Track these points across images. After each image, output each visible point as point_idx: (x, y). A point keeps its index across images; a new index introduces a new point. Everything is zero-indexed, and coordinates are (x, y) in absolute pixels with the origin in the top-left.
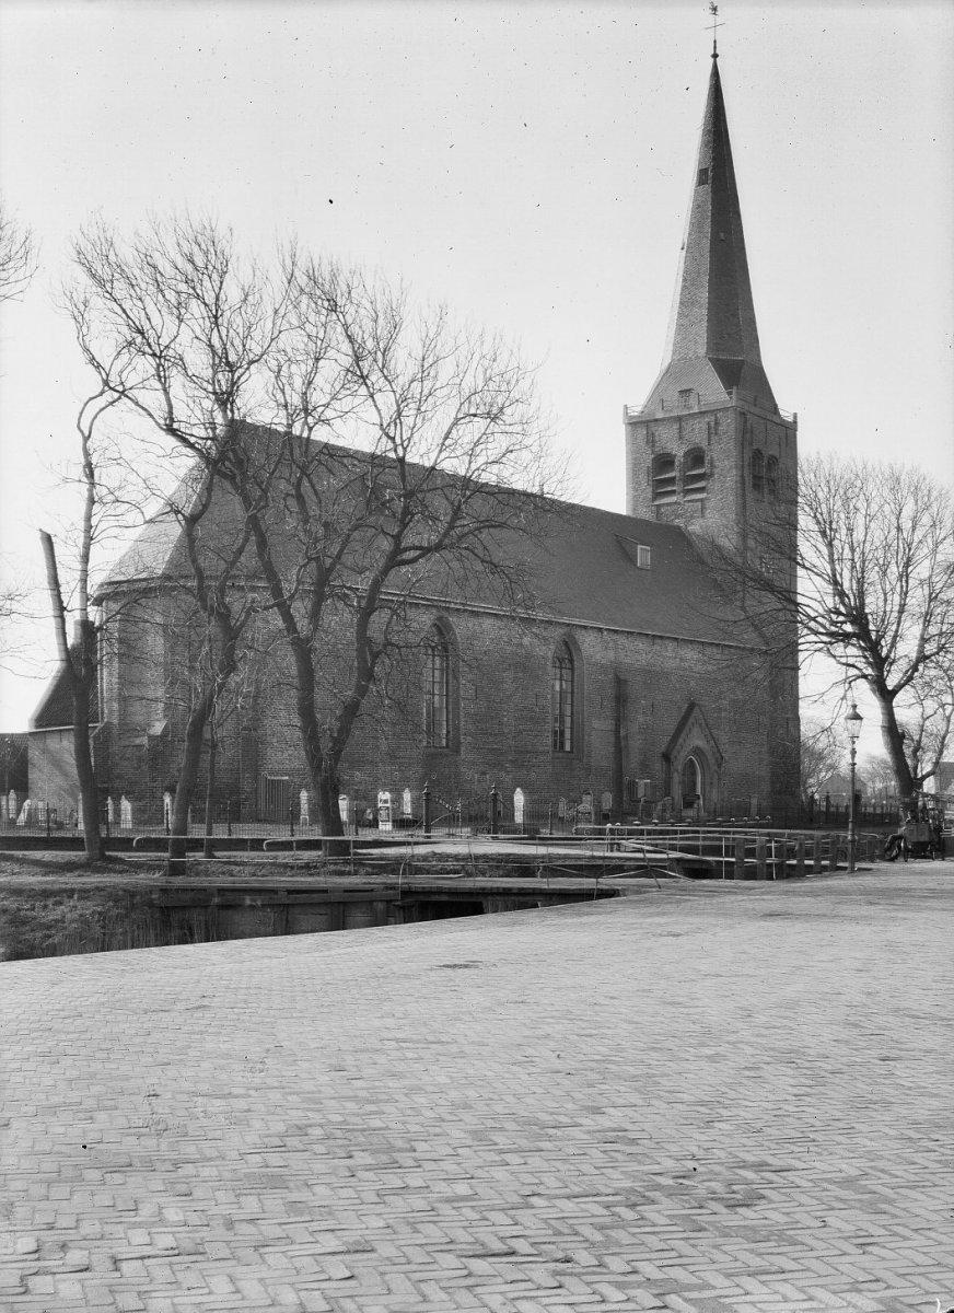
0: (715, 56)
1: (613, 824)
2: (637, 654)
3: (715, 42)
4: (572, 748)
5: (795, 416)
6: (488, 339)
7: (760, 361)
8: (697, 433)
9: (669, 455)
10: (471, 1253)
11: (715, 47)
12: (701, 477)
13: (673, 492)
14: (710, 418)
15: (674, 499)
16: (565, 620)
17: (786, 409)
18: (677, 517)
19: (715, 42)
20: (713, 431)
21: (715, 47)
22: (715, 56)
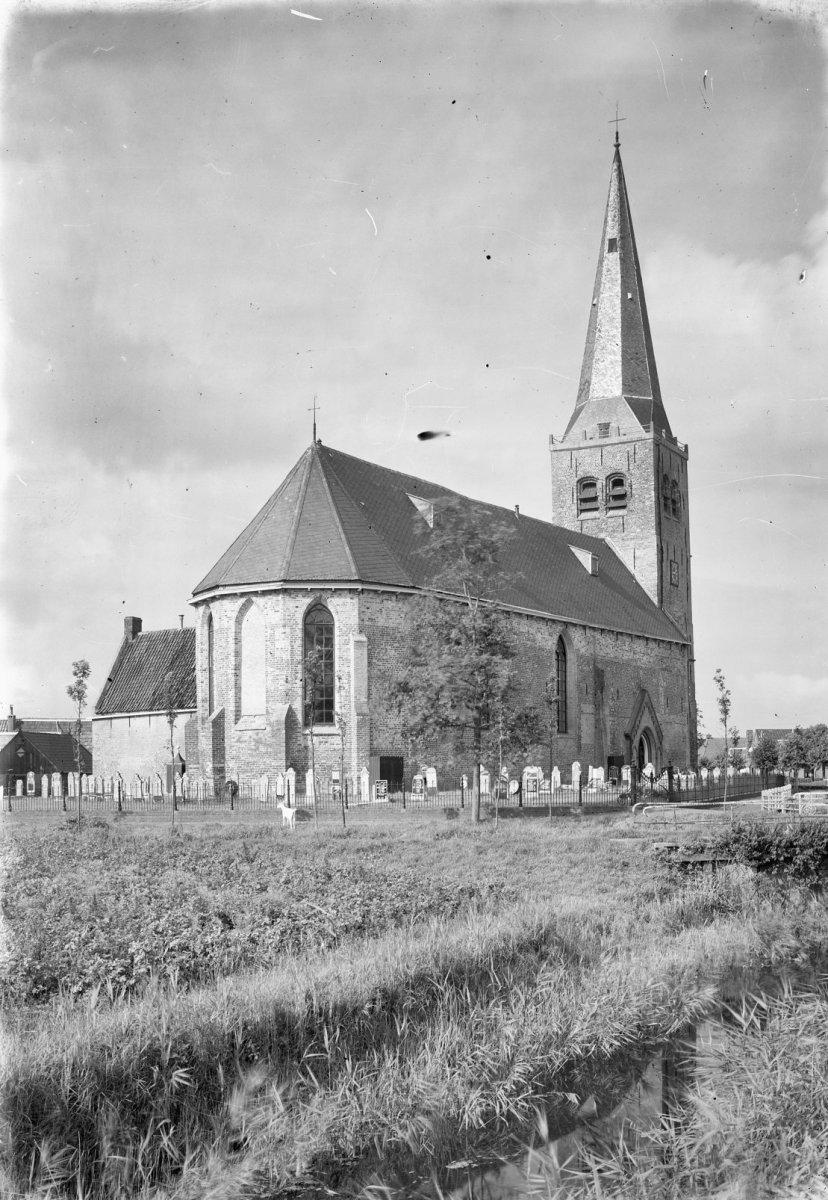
0: (617, 146)
1: (76, 756)
2: (608, 648)
3: (617, 133)
4: (14, 784)
5: (686, 446)
6: (184, 989)
7: (661, 402)
8: (617, 462)
9: (591, 478)
10: (206, 627)
11: (617, 138)
12: (622, 497)
13: (596, 509)
14: (629, 448)
15: (595, 514)
16: (565, 619)
17: (681, 442)
18: (601, 530)
19: (617, 133)
20: (630, 458)
21: (617, 138)
22: (617, 146)
